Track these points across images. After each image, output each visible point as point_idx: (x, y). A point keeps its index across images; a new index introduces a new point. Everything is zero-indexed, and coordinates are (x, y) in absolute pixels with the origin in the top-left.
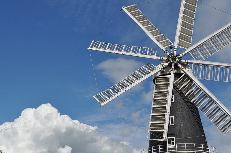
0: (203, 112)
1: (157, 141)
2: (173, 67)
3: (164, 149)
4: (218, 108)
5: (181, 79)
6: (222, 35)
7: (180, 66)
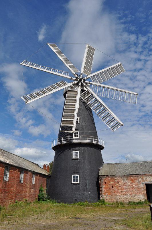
0: (99, 116)
2: (80, 85)
4: (109, 114)
5: (84, 94)
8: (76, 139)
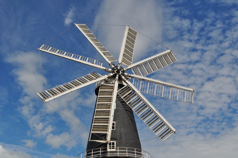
1: (97, 142)
2: (117, 78)
3: (105, 152)
4: (157, 118)
5: (122, 90)
6: (157, 60)
7: (123, 77)
8: (111, 152)
